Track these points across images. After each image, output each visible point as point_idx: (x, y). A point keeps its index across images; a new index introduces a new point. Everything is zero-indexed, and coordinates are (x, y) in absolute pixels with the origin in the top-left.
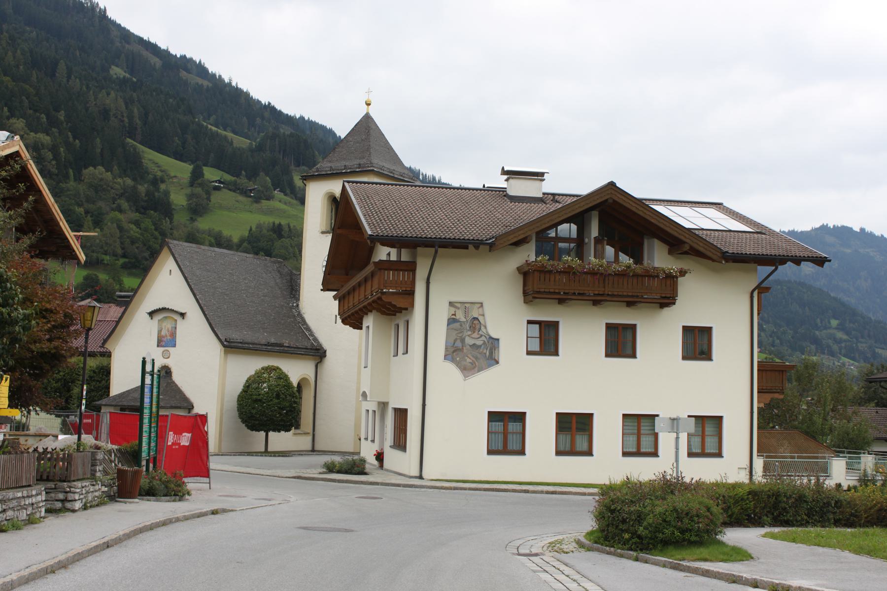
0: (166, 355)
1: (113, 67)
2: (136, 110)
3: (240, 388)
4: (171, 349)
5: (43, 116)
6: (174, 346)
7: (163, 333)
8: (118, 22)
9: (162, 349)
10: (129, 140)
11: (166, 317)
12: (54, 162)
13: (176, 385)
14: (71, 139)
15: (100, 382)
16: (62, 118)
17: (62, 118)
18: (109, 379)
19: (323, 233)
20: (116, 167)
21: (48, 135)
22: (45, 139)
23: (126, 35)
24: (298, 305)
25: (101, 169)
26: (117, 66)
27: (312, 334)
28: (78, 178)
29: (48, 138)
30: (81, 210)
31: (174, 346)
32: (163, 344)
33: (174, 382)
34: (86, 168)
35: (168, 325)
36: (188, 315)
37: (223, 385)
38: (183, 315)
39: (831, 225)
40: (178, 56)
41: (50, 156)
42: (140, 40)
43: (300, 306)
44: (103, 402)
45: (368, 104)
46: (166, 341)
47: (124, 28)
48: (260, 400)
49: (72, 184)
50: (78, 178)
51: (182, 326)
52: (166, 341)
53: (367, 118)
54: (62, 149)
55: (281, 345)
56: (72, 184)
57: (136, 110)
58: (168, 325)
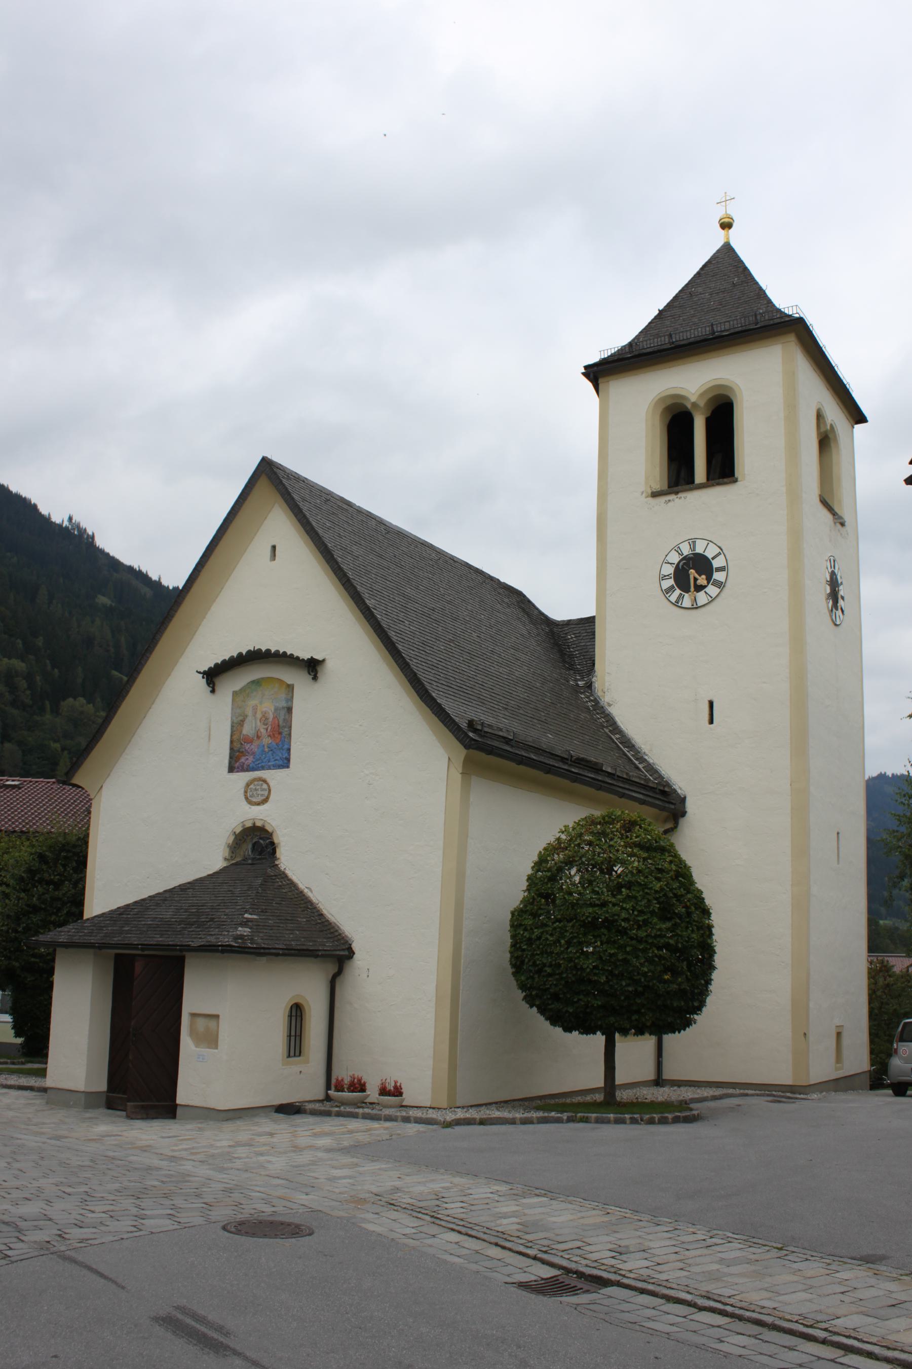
0: (257, 795)
1: (99, 596)
2: (123, 639)
3: (515, 892)
4: (274, 776)
5: (19, 641)
6: (285, 763)
7: (248, 729)
8: (107, 550)
9: (243, 778)
10: (115, 673)
11: (257, 683)
12: (28, 692)
13: (292, 885)
14: (49, 668)
15: (58, 886)
16: (40, 644)
17: (40, 644)
18: (83, 879)
19: (655, 495)
20: (99, 699)
21: (23, 661)
22: (19, 665)
23: (114, 564)
24: (589, 686)
25: (82, 700)
26: (104, 595)
27: (642, 760)
28: (56, 711)
29: (23, 665)
30: (57, 746)
31: (285, 763)
32: (249, 760)
33: (284, 876)
34: (64, 700)
35: (266, 704)
36: (331, 665)
37: (457, 878)
38: (313, 666)
39: (889, 774)
40: (171, 588)
41: (23, 684)
42: (130, 569)
43: (597, 685)
44: (62, 934)
45: (726, 225)
46: (258, 752)
47: (113, 558)
48: (609, 923)
49: (48, 717)
50: (56, 711)
51: (308, 701)
52: (258, 752)
53: (727, 250)
54: (38, 678)
55: (596, 768)
56: (48, 717)
57: (123, 639)
58: (266, 704)
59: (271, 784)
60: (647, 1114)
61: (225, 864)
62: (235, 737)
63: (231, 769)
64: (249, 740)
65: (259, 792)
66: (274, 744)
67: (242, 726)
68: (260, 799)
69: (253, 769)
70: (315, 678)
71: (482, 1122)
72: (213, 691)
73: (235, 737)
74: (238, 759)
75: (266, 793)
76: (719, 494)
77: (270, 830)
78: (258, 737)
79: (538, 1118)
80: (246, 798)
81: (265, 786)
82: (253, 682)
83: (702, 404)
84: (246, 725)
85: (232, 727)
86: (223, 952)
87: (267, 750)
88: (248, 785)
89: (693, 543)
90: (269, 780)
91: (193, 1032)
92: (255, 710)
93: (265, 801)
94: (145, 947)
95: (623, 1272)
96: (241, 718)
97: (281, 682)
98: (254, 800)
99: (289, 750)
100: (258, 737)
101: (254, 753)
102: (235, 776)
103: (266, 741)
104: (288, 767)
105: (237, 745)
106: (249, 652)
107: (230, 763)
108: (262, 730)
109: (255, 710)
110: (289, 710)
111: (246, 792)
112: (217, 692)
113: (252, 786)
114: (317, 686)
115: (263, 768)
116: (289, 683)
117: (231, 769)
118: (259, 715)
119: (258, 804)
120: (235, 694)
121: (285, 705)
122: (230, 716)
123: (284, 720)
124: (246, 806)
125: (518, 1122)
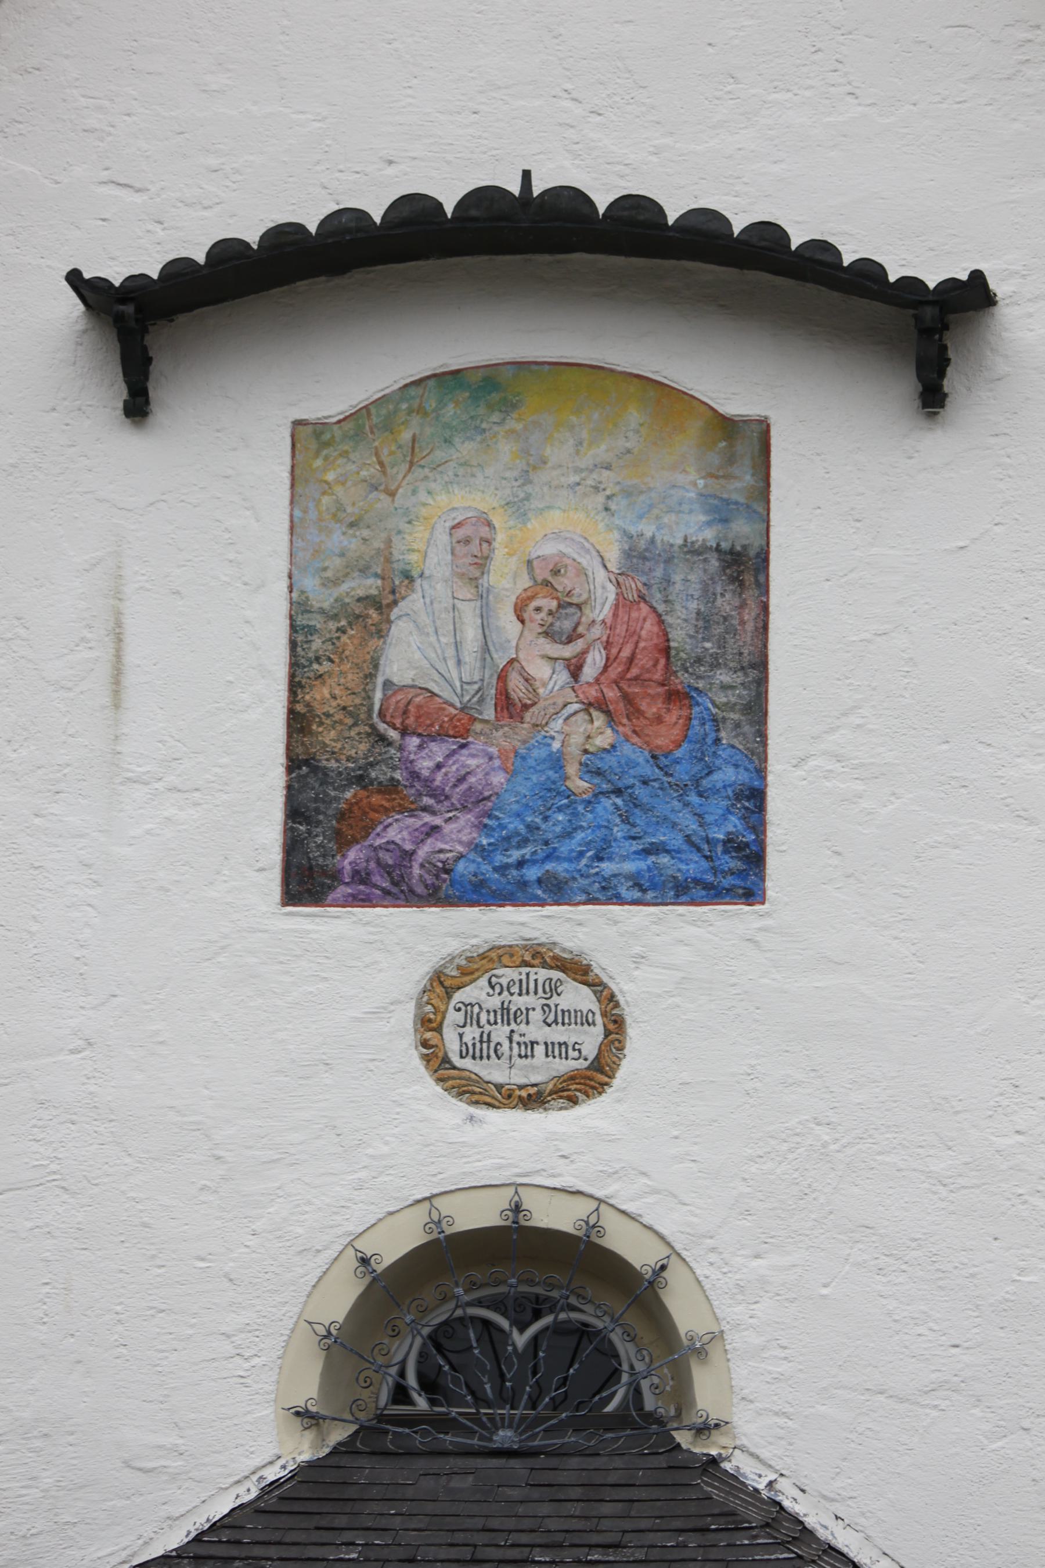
4: (648, 950)
6: (736, 870)
7: (422, 652)
11: (489, 390)
59: (627, 988)
60: (491, 1387)
61: (304, 1449)
62: (320, 696)
63: (305, 882)
64: (423, 717)
65: (536, 1031)
67: (380, 632)
68: (541, 1070)
69: (480, 894)
70: (932, 398)
72: (137, 407)
73: (319, 695)
74: (353, 826)
75: (591, 1039)
77: (638, 1253)
78: (509, 707)
80: (438, 1063)
81: (576, 997)
82: (449, 380)
84: (400, 630)
85: (298, 633)
87: (580, 785)
88: (442, 984)
90: (605, 963)
92: (474, 548)
93: (592, 1079)
95: (88, 1521)
96: (370, 585)
97: (666, 400)
98: (494, 1072)
99: (753, 799)
101: (478, 801)
102: (337, 928)
103: (578, 734)
104: (751, 894)
106: (483, 200)
107: (292, 846)
108: (540, 670)
109: (474, 548)
110: (745, 568)
111: (429, 1024)
112: (159, 415)
113: (476, 992)
114: (937, 444)
115: (556, 891)
116: (731, 408)
117: (305, 882)
118: (506, 579)
119: (533, 1099)
120: (309, 439)
121: (709, 536)
122: (281, 565)
123: (705, 621)
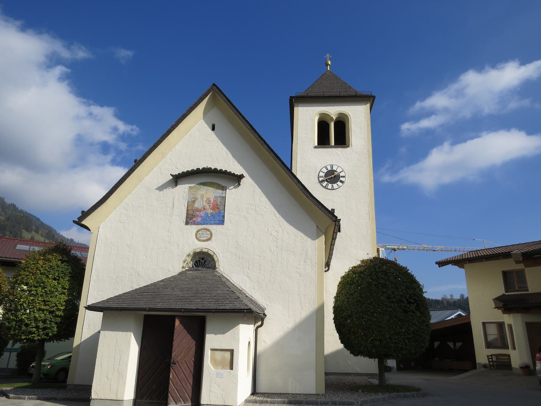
6: (221, 222)
7: (197, 205)
9: (194, 229)
31: (221, 222)
40: (19, 209)
62: (189, 208)
63: (187, 223)
65: (205, 235)
66: (214, 213)
68: (205, 238)
69: (201, 224)
71: (271, 403)
75: (209, 236)
76: (339, 151)
78: (204, 209)
79: (259, 400)
81: (208, 232)
83: (334, 118)
86: (214, 312)
87: (210, 215)
88: (198, 232)
89: (332, 166)
91: (215, 362)
92: (202, 197)
94: (179, 310)
98: (201, 239)
100: (204, 209)
102: (189, 227)
104: (223, 224)
105: (191, 212)
109: (202, 197)
113: (200, 232)
115: (207, 224)
117: (187, 223)
118: (205, 199)
124: (196, 241)
125: (304, 403)
